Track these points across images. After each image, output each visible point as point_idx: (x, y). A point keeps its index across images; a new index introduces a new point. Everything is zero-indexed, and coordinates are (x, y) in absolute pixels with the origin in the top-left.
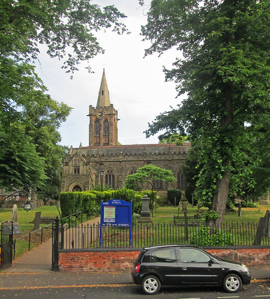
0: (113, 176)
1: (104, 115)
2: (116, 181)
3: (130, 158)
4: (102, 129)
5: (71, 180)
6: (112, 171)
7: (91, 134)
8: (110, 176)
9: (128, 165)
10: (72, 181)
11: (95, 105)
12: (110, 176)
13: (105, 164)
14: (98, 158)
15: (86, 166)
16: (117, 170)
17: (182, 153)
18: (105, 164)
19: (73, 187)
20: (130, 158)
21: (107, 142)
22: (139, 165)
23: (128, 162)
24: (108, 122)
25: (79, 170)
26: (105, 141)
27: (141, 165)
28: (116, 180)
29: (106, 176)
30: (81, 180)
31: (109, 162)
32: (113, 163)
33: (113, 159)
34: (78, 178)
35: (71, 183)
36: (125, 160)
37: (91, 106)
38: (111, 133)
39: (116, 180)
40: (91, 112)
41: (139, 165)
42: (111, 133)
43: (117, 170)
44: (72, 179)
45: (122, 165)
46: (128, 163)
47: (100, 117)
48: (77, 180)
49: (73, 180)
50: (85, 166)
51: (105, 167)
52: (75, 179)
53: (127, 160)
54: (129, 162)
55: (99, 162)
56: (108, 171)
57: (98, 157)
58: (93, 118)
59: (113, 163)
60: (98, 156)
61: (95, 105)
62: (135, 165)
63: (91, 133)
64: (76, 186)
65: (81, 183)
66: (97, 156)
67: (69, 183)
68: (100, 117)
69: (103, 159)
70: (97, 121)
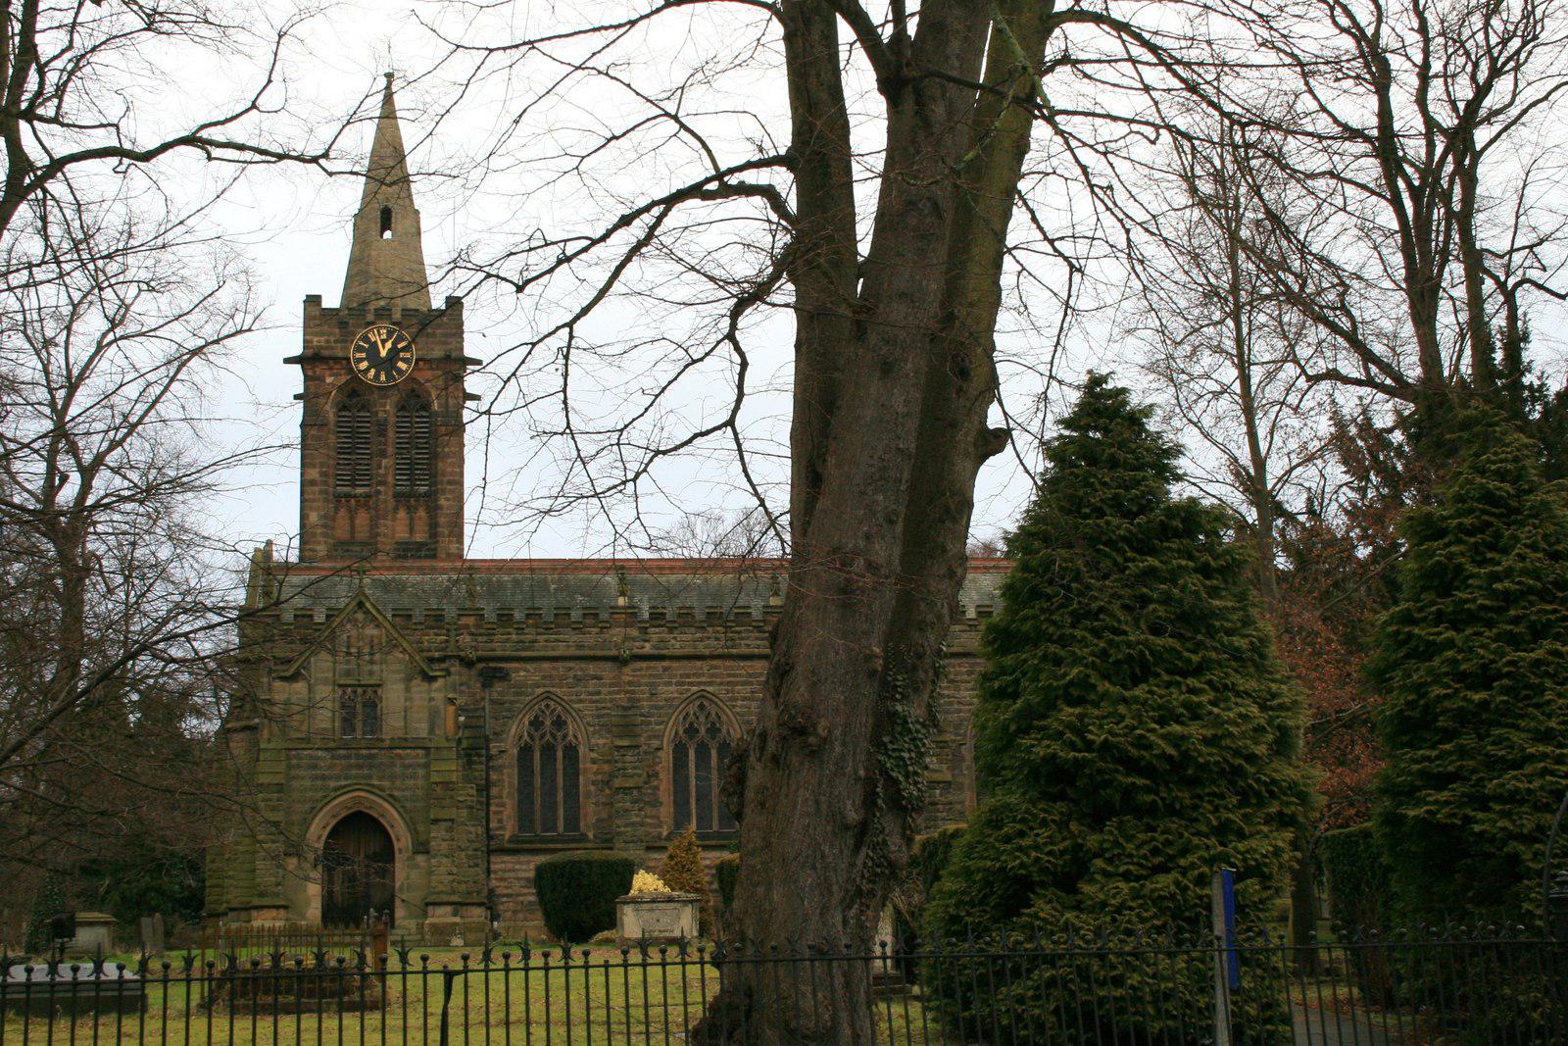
0: (571, 752)
1: (405, 360)
2: (592, 788)
3: (680, 642)
4: (391, 450)
5: (324, 778)
6: (559, 723)
7: (313, 483)
8: (548, 750)
9: (669, 684)
10: (332, 784)
11: (332, 300)
12: (548, 750)
13: (521, 673)
14: (472, 634)
15: (425, 685)
16: (598, 717)
17: (422, 619)
18: (521, 673)
19: (334, 822)
20: (680, 642)
21: (419, 537)
22: (737, 684)
23: (666, 664)
24: (426, 407)
25: (372, 705)
26: (411, 531)
27: (751, 683)
28: (594, 783)
29: (525, 752)
30: (393, 778)
31: (546, 665)
32: (570, 669)
33: (567, 642)
34: (371, 766)
35: (321, 794)
36: (648, 648)
37: (313, 301)
38: (450, 483)
39: (594, 783)
40: (315, 340)
41: (737, 684)
42: (450, 483)
43: (598, 717)
44: (330, 768)
45: (630, 683)
46: (665, 669)
47: (377, 376)
48: (364, 777)
49: (338, 778)
50: (418, 681)
51: (517, 694)
52: (350, 766)
53: (665, 652)
54: (676, 664)
55: (481, 659)
56: (536, 723)
57: (467, 626)
58: (329, 380)
59: (570, 669)
60: (471, 621)
61: (332, 300)
62: (710, 684)
63: (314, 474)
64: (338, 823)
65: (396, 793)
66: (464, 621)
67: (310, 794)
68: (368, 370)
69: (502, 644)
70: (355, 393)
